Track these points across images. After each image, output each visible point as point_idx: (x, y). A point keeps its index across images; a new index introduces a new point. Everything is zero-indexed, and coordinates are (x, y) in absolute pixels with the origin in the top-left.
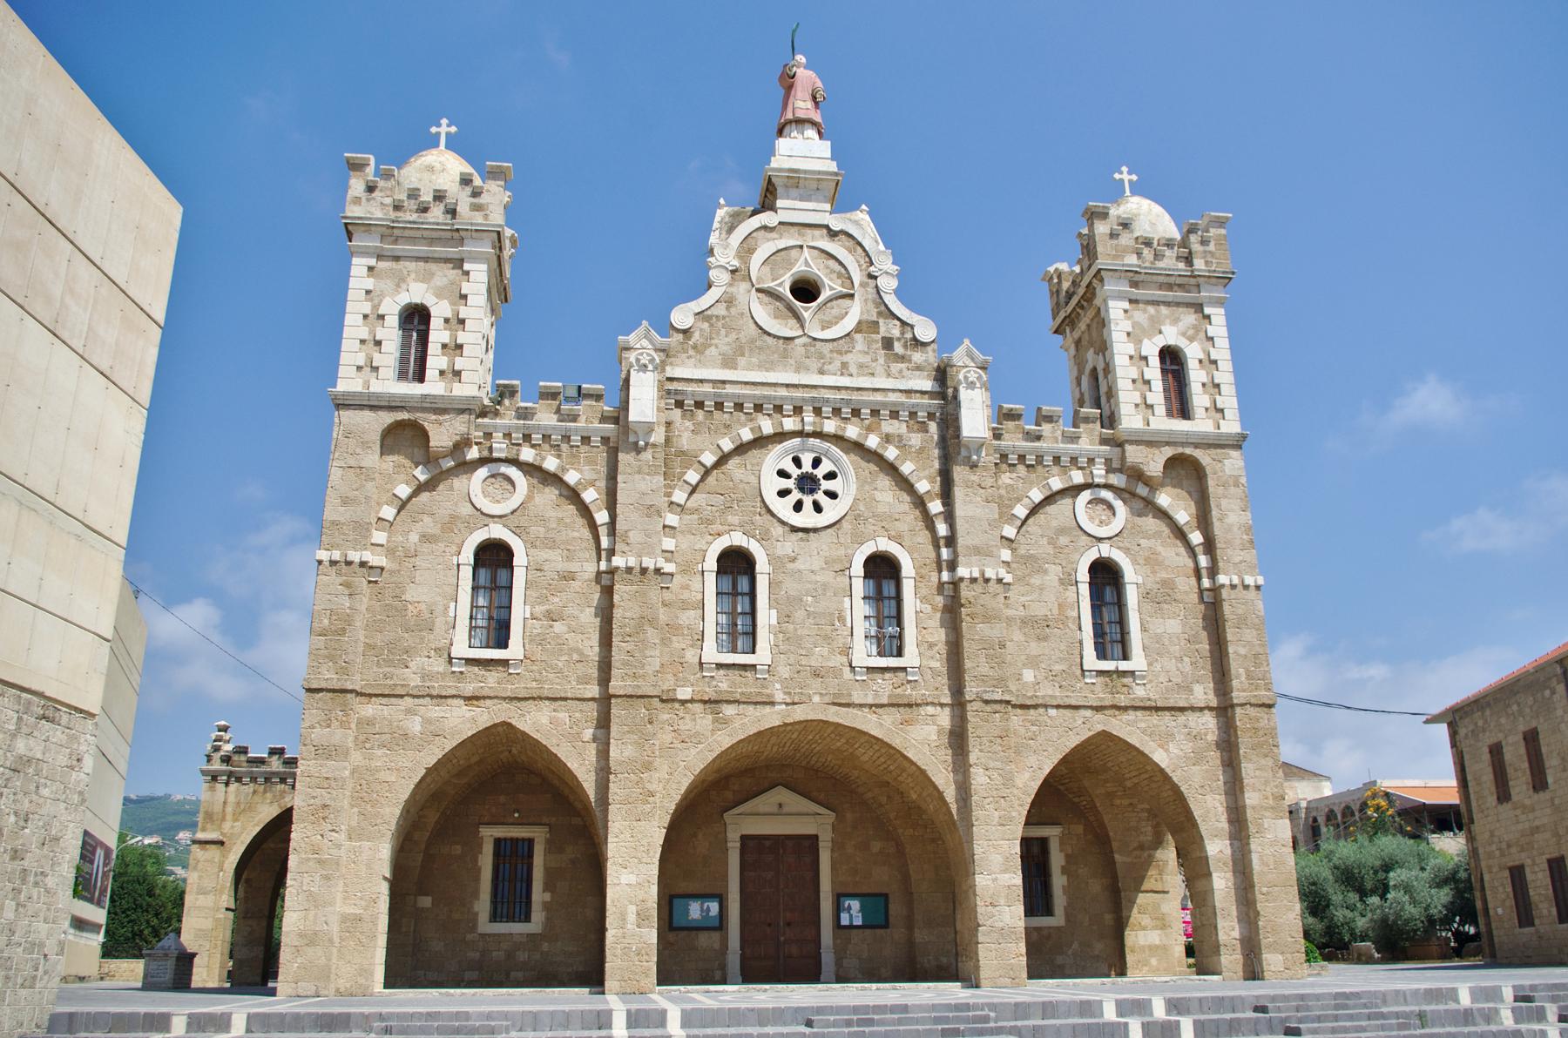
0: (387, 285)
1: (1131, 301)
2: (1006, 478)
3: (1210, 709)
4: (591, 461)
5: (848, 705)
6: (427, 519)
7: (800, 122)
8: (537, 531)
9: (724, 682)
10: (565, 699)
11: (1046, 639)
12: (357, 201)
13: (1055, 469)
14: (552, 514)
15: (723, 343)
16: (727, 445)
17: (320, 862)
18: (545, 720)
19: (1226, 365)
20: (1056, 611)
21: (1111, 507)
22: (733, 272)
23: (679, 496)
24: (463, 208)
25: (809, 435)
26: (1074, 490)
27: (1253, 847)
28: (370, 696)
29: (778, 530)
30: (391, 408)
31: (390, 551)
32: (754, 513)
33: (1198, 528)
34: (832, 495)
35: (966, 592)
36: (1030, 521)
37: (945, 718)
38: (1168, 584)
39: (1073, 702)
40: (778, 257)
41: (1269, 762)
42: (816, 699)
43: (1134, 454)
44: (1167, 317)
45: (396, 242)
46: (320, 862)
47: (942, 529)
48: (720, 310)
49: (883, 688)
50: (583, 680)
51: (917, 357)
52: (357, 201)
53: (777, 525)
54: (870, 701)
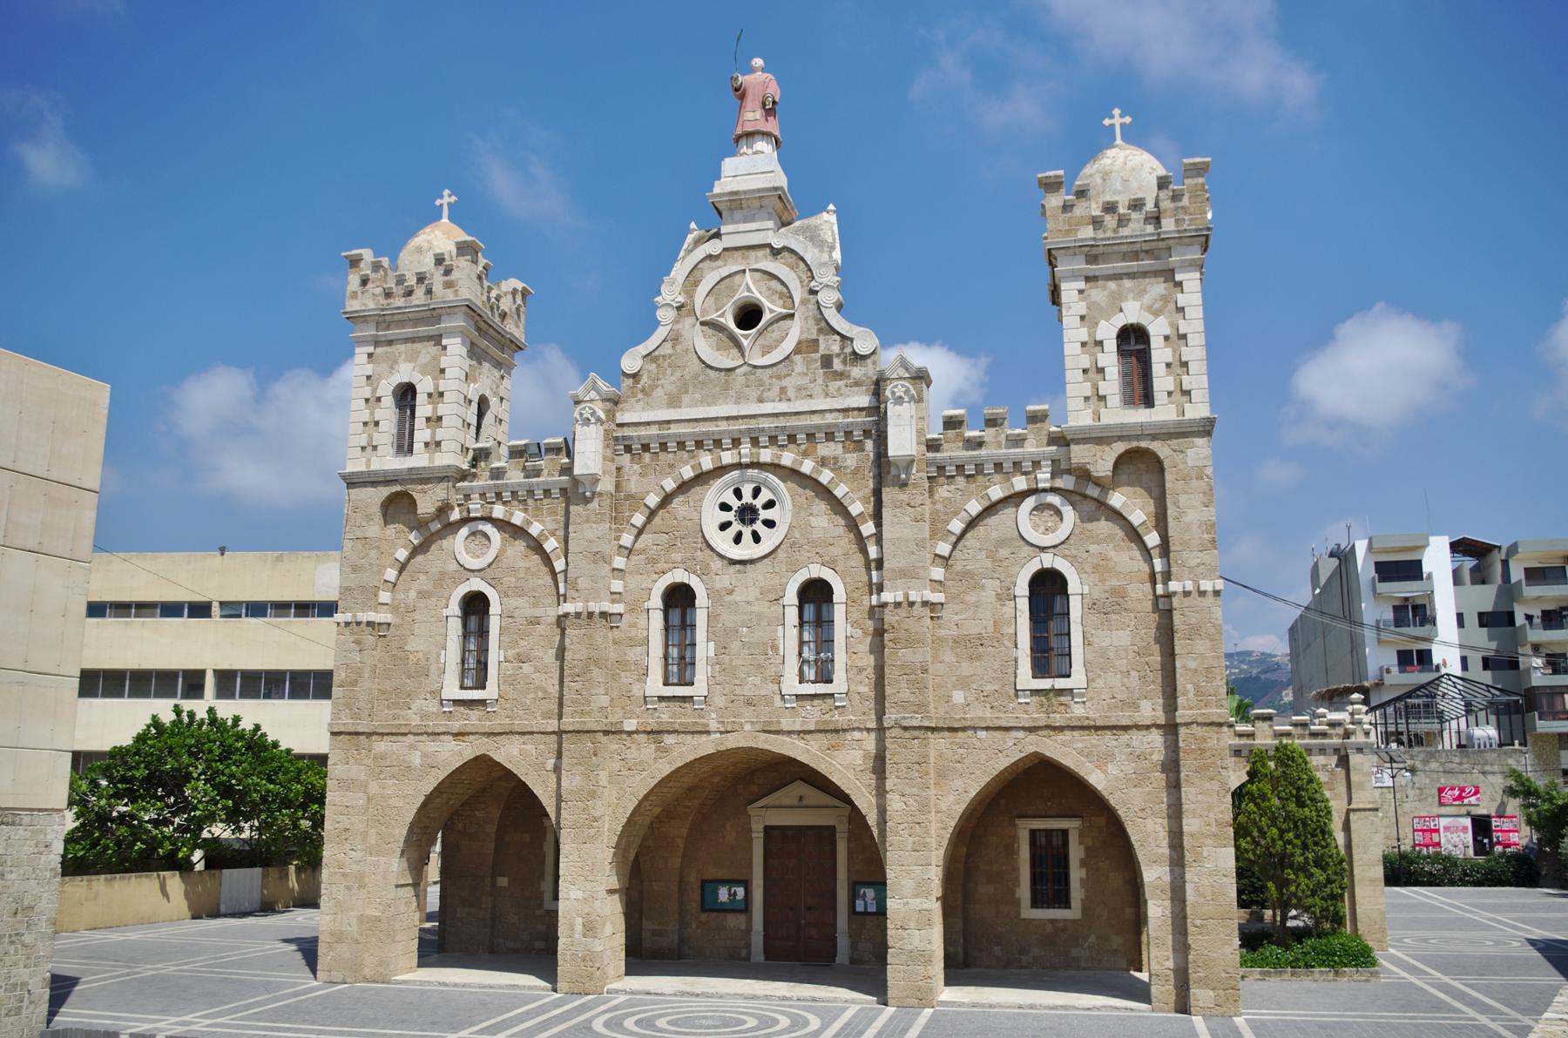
0: (383, 368)
1: (1088, 279)
2: (943, 491)
3: (1158, 726)
4: (553, 513)
5: (777, 732)
6: (422, 577)
7: (750, 135)
8: (510, 580)
9: (665, 715)
10: (532, 733)
11: (979, 658)
12: (354, 295)
13: (997, 478)
14: (521, 564)
15: (669, 382)
16: (670, 485)
17: (344, 875)
18: (516, 752)
19: (1197, 339)
20: (990, 629)
21: (1058, 512)
22: (679, 308)
23: (627, 539)
24: (438, 288)
25: (748, 466)
26: (1016, 498)
27: (1188, 876)
28: (383, 734)
29: (717, 564)
30: (387, 483)
31: (393, 607)
32: (695, 549)
33: (1156, 528)
34: (770, 524)
35: (890, 617)
36: (968, 535)
37: (870, 742)
38: (1118, 593)
39: (1004, 724)
40: (722, 286)
41: (1215, 785)
42: (747, 727)
43: (1079, 454)
44: (1131, 290)
45: (388, 328)
46: (344, 875)
47: (873, 552)
48: (667, 349)
49: (812, 715)
50: (547, 716)
51: (857, 372)
52: (354, 295)
53: (716, 558)
54: (798, 727)
